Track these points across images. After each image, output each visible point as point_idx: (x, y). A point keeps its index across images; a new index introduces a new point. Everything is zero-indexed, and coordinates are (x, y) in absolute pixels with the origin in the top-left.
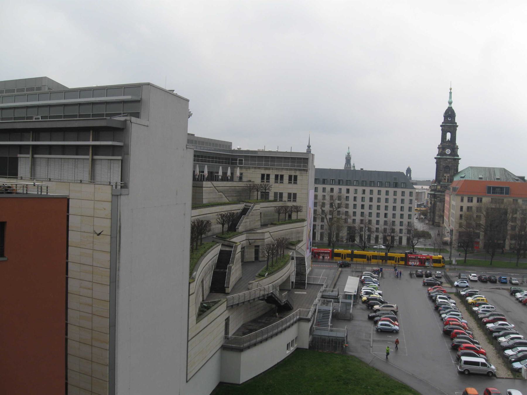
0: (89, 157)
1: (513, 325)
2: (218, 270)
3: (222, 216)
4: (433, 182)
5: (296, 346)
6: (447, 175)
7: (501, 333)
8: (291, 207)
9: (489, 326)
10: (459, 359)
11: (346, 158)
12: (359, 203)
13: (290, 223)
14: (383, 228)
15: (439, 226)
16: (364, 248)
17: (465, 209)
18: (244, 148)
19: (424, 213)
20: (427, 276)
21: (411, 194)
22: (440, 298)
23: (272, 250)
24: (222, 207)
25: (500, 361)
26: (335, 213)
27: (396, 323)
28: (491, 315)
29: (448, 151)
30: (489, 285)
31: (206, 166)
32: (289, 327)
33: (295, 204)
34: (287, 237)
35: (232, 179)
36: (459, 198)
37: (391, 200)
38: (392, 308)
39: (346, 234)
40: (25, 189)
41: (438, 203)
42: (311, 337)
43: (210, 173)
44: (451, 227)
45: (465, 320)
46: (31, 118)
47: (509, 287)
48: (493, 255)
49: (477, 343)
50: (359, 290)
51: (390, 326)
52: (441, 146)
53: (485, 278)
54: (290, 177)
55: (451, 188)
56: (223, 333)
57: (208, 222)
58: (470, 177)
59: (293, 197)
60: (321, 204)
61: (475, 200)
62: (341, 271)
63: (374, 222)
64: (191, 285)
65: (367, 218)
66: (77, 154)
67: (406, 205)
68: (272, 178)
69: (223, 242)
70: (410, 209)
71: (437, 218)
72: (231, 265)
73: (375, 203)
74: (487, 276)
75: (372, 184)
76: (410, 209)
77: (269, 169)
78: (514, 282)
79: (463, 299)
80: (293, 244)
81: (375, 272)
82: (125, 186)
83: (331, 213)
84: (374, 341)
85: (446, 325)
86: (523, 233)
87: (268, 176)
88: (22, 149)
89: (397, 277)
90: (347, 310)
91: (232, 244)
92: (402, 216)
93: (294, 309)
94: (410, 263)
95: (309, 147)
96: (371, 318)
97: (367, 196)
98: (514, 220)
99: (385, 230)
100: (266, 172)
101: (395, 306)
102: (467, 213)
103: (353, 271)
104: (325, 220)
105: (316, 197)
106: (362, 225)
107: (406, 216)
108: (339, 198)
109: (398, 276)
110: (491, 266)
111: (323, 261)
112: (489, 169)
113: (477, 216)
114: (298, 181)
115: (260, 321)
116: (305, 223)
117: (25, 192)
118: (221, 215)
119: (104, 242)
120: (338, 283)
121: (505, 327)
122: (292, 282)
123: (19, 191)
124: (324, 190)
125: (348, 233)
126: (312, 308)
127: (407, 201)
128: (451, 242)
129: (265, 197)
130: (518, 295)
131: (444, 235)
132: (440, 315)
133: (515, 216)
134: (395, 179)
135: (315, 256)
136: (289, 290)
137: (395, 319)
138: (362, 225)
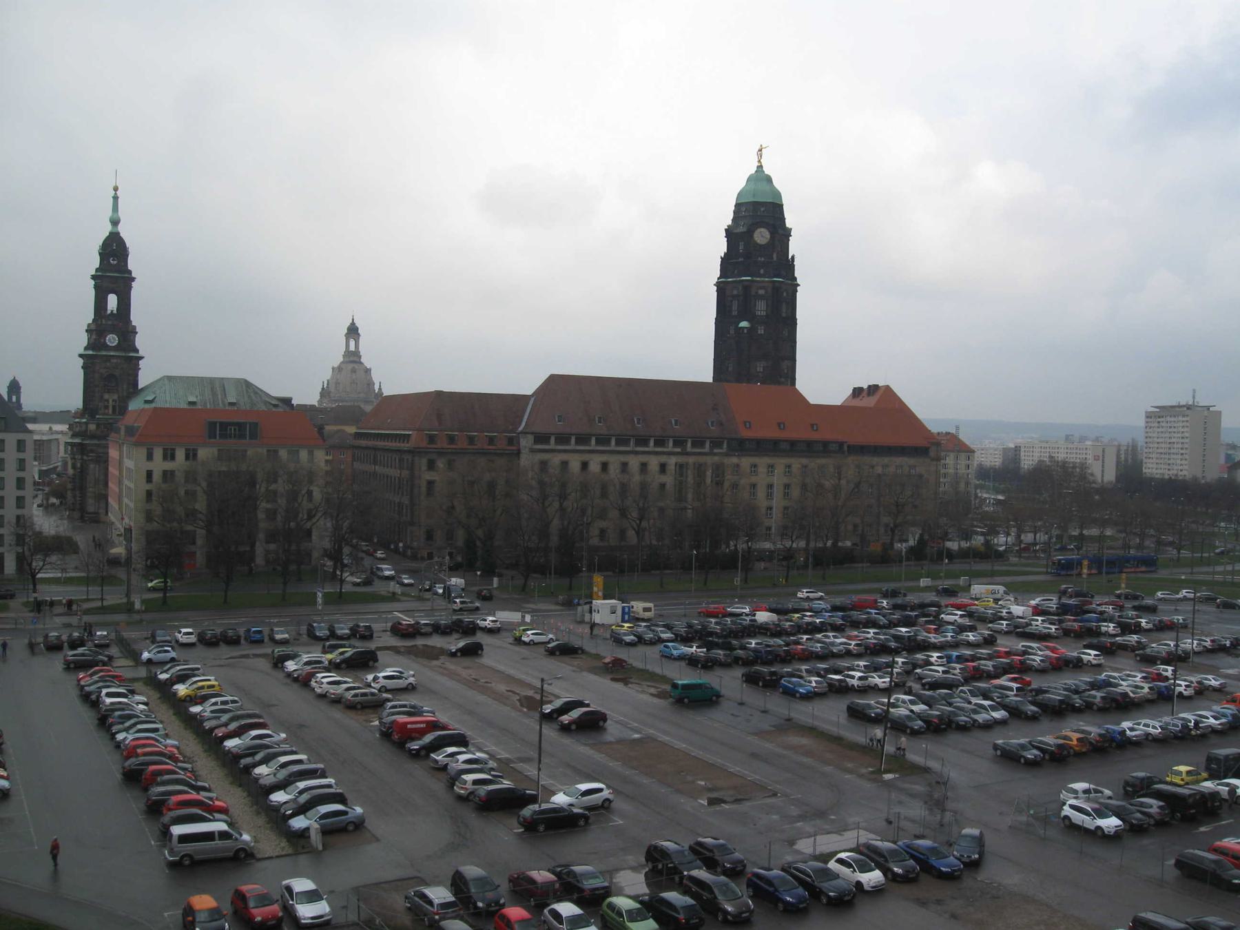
1: (283, 735)
6: (111, 398)
7: (258, 757)
9: (231, 743)
10: (165, 833)
17: (157, 477)
20: (74, 645)
21: (21, 445)
25: (261, 820)
30: (225, 651)
44: (126, 520)
45: (173, 739)
47: (269, 651)
52: (93, 327)
53: (215, 636)
58: (167, 400)
61: (180, 454)
71: (90, 501)
74: (218, 631)
78: (278, 637)
79: (164, 690)
85: (127, 758)
86: (292, 524)
98: (272, 496)
102: (164, 486)
112: (212, 381)
113: (187, 492)
121: (266, 741)
130: (291, 666)
132: (113, 736)
133: (273, 487)
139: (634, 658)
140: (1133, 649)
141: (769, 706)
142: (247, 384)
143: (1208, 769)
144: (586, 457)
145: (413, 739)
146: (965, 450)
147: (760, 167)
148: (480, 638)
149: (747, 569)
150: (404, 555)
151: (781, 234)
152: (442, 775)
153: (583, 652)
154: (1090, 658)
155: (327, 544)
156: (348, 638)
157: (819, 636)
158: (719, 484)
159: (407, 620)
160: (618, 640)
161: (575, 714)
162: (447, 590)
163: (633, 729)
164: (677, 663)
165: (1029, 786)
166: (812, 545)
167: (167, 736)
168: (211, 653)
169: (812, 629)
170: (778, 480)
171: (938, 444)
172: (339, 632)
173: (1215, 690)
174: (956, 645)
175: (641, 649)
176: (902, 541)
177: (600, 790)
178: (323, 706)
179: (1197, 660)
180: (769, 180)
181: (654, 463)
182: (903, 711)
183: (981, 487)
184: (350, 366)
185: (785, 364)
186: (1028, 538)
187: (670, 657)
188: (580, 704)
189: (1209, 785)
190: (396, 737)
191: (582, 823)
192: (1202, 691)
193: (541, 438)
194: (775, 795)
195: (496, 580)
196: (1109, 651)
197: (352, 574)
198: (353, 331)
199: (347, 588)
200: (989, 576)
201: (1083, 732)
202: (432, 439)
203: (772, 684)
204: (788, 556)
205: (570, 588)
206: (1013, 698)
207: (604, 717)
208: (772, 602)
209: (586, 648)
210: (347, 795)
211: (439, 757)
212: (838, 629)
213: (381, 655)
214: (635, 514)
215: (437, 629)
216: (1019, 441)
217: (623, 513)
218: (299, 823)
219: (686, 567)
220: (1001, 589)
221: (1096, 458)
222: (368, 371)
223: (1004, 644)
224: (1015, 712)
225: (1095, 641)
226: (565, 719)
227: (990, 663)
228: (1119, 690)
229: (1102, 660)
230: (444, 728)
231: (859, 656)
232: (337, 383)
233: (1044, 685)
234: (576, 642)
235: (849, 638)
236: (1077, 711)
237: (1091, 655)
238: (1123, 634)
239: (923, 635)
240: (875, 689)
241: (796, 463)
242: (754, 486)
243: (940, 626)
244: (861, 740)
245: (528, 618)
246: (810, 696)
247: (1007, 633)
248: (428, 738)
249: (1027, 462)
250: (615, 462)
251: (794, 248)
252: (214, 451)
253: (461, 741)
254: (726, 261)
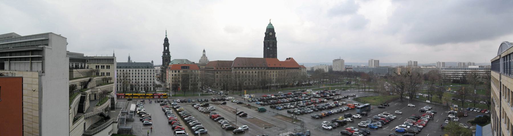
0: (30, 61)
1: (194, 118)
2: (80, 104)
3: (81, 83)
4: (161, 66)
5: (112, 133)
6: (167, 63)
7: (190, 121)
8: (108, 78)
9: (185, 119)
10: (175, 133)
11: (128, 58)
12: (134, 75)
13: (108, 84)
14: (144, 84)
15: (165, 82)
16: (137, 93)
17: (174, 75)
18: (89, 56)
19: (159, 78)
20: (161, 102)
21: (154, 70)
22: (167, 110)
23: (101, 95)
24: (81, 79)
25: (190, 131)
26: (125, 80)
27: (151, 121)
28: (186, 115)
29: (166, 54)
30: (184, 103)
31: (74, 63)
32: (109, 125)
33: (109, 77)
34: (107, 90)
35: (84, 68)
36: (172, 71)
37: (146, 74)
38: (149, 115)
39: (130, 87)
40: (7, 74)
41: (164, 74)
42: (118, 129)
43: (76, 66)
44: (169, 82)
45: (177, 117)
46: (9, 48)
47: (191, 103)
48: (185, 92)
49: (181, 126)
50: (136, 109)
51: (148, 122)
53: (183, 101)
54: (107, 66)
55: (168, 68)
56: (83, 129)
57: (76, 85)
58: (175, 63)
59: (108, 74)
60: (119, 76)
61: (177, 71)
62: (129, 102)
63: (140, 82)
64: (70, 110)
65: (138, 81)
66: (25, 61)
67: (152, 75)
68: (100, 67)
69: (82, 93)
70: (154, 76)
71: (164, 79)
72: (85, 102)
73: (140, 75)
74: (183, 100)
75: (139, 67)
76: (154, 76)
77: (99, 63)
78: (193, 101)
79: (175, 109)
80: (109, 92)
81: (141, 102)
82: (43, 72)
83: (124, 79)
84: (142, 129)
85: (169, 120)
86: (195, 83)
87: (98, 66)
88: (6, 59)
89: (150, 103)
90: (132, 117)
91: (85, 93)
92: (151, 79)
93: (111, 118)
94: (155, 97)
95: (114, 54)
96: (141, 120)
97: (137, 72)
98: (191, 78)
99: (145, 85)
100: (98, 65)
101: (150, 114)
102: (175, 77)
103: (133, 102)
104: (121, 83)
105: (117, 73)
106: (136, 84)
107: (152, 79)
108: (127, 74)
109: (151, 103)
110: (184, 96)
111: (121, 98)
112: (182, 60)
113: (178, 78)
114: (110, 68)
115: (98, 124)
116: (114, 84)
117: (7, 75)
118: (81, 82)
119: (36, 94)
120: (128, 107)
121: (191, 118)
122: (110, 108)
123: (5, 75)
124: (120, 71)
125: (131, 87)
126: (118, 117)
127: (152, 74)
128: (170, 88)
129: (98, 74)
130: (195, 106)
131: (167, 86)
132: (167, 116)
133: (192, 77)
134: (147, 65)
135: (118, 97)
136: (108, 111)
137: (150, 120)
138: (136, 84)
139: (252, 104)
140: (332, 99)
141: (274, 112)
142: (187, 60)
143: (344, 117)
144: (243, 71)
145: (215, 118)
146: (305, 68)
147: (270, 23)
148: (226, 101)
149: (270, 89)
150: (213, 87)
151: (274, 34)
152: (220, 125)
153: (243, 103)
154: (325, 101)
155: (200, 86)
156: (204, 101)
157: (282, 99)
158: (265, 75)
159: (214, 98)
160: (249, 101)
161: (242, 114)
162: (220, 93)
163: (252, 116)
164: (259, 105)
165: (317, 122)
166: (281, 84)
167: (175, 117)
168: (182, 104)
169: (281, 98)
170: (275, 74)
171: (300, 67)
172: (203, 100)
173: (345, 104)
174: (304, 100)
175: (253, 103)
176: (295, 83)
177: (246, 127)
178: (200, 113)
179: (342, 99)
180: (272, 25)
181: (254, 71)
182: (296, 111)
183: (308, 74)
184: (204, 57)
185: (275, 55)
186: (315, 82)
187: (258, 104)
188: (243, 112)
189: (345, 119)
190: (212, 118)
191: (243, 132)
192: (343, 105)
193: (235, 68)
194: (276, 126)
195: (228, 92)
196: (328, 99)
197: (205, 91)
198: (204, 51)
199: (204, 93)
200: (309, 88)
201: (325, 113)
202: (217, 68)
203: (275, 108)
204: (277, 86)
205: (241, 93)
206: (314, 108)
207: (247, 114)
208: (274, 94)
209: (243, 103)
210: (204, 128)
211: (219, 121)
212: (285, 98)
213: (209, 104)
214: (251, 80)
215: (219, 100)
216: (313, 66)
217: (249, 80)
218: (197, 132)
219: (260, 89)
220: (311, 90)
221: (325, 68)
222: (207, 57)
223: (312, 99)
224: (314, 110)
225: (326, 98)
226: (240, 115)
227: (310, 102)
228: (330, 105)
229: (327, 101)
230: (220, 116)
231: (289, 102)
232: (202, 60)
233: (319, 105)
234: (242, 102)
235: (287, 100)
236: (324, 109)
237: (325, 100)
238: (330, 96)
239: (299, 98)
240: (292, 108)
241: (278, 71)
242: (271, 75)
243: (302, 97)
244: (290, 116)
245: (234, 98)
246: (281, 110)
247: (313, 97)
248: (218, 118)
249: (315, 70)
250: (248, 71)
251: (276, 35)
252: (182, 71)
253: (223, 119)
254: (265, 38)
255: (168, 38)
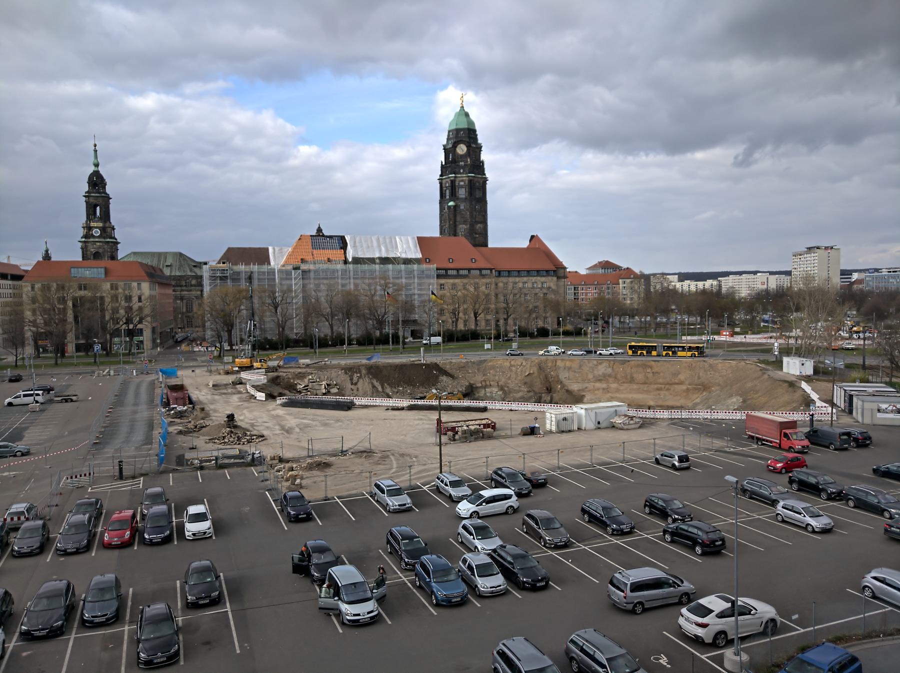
52: (85, 225)
142: (181, 254)
255: (101, 172)
